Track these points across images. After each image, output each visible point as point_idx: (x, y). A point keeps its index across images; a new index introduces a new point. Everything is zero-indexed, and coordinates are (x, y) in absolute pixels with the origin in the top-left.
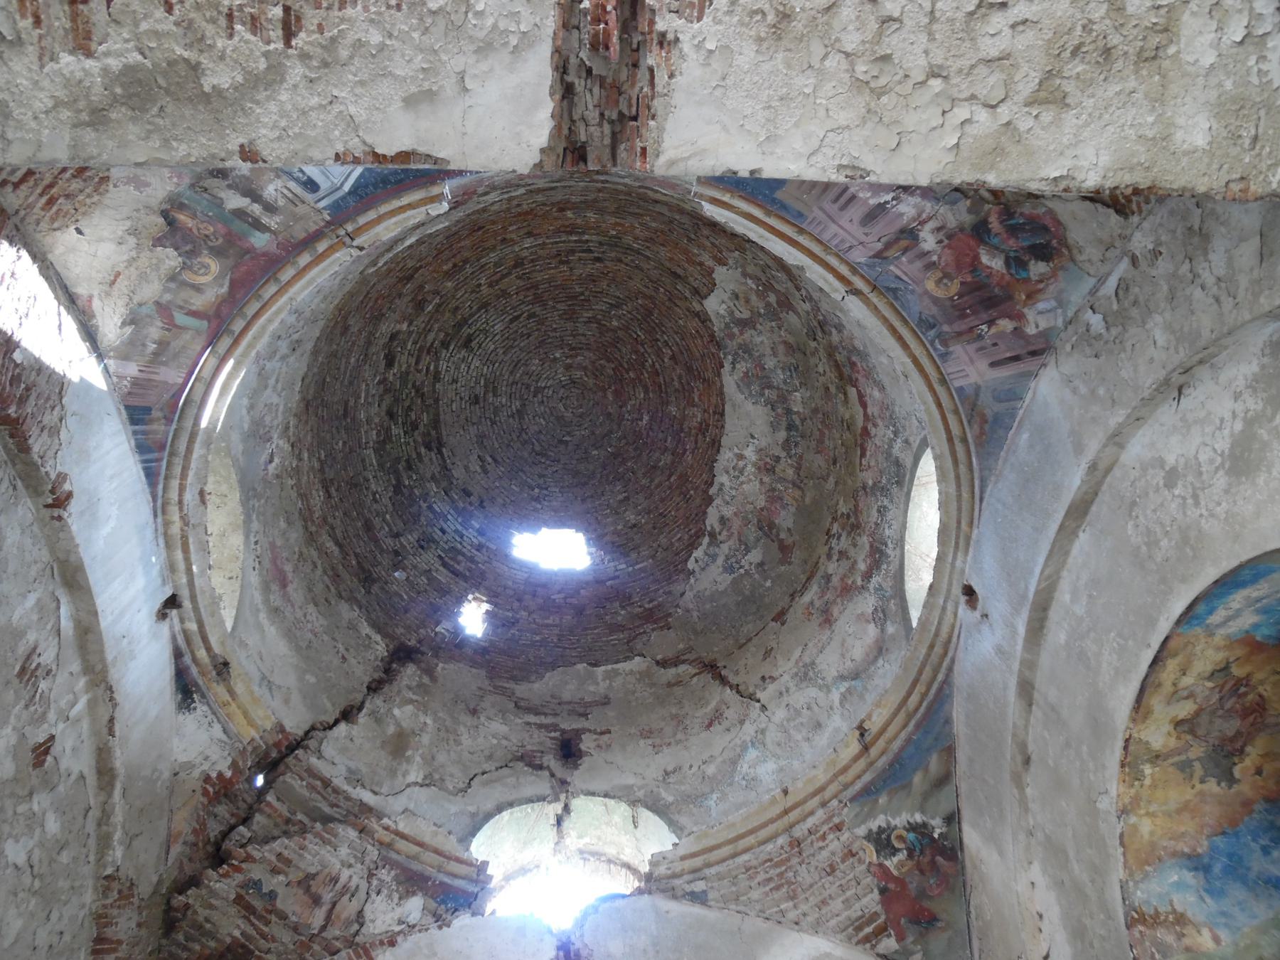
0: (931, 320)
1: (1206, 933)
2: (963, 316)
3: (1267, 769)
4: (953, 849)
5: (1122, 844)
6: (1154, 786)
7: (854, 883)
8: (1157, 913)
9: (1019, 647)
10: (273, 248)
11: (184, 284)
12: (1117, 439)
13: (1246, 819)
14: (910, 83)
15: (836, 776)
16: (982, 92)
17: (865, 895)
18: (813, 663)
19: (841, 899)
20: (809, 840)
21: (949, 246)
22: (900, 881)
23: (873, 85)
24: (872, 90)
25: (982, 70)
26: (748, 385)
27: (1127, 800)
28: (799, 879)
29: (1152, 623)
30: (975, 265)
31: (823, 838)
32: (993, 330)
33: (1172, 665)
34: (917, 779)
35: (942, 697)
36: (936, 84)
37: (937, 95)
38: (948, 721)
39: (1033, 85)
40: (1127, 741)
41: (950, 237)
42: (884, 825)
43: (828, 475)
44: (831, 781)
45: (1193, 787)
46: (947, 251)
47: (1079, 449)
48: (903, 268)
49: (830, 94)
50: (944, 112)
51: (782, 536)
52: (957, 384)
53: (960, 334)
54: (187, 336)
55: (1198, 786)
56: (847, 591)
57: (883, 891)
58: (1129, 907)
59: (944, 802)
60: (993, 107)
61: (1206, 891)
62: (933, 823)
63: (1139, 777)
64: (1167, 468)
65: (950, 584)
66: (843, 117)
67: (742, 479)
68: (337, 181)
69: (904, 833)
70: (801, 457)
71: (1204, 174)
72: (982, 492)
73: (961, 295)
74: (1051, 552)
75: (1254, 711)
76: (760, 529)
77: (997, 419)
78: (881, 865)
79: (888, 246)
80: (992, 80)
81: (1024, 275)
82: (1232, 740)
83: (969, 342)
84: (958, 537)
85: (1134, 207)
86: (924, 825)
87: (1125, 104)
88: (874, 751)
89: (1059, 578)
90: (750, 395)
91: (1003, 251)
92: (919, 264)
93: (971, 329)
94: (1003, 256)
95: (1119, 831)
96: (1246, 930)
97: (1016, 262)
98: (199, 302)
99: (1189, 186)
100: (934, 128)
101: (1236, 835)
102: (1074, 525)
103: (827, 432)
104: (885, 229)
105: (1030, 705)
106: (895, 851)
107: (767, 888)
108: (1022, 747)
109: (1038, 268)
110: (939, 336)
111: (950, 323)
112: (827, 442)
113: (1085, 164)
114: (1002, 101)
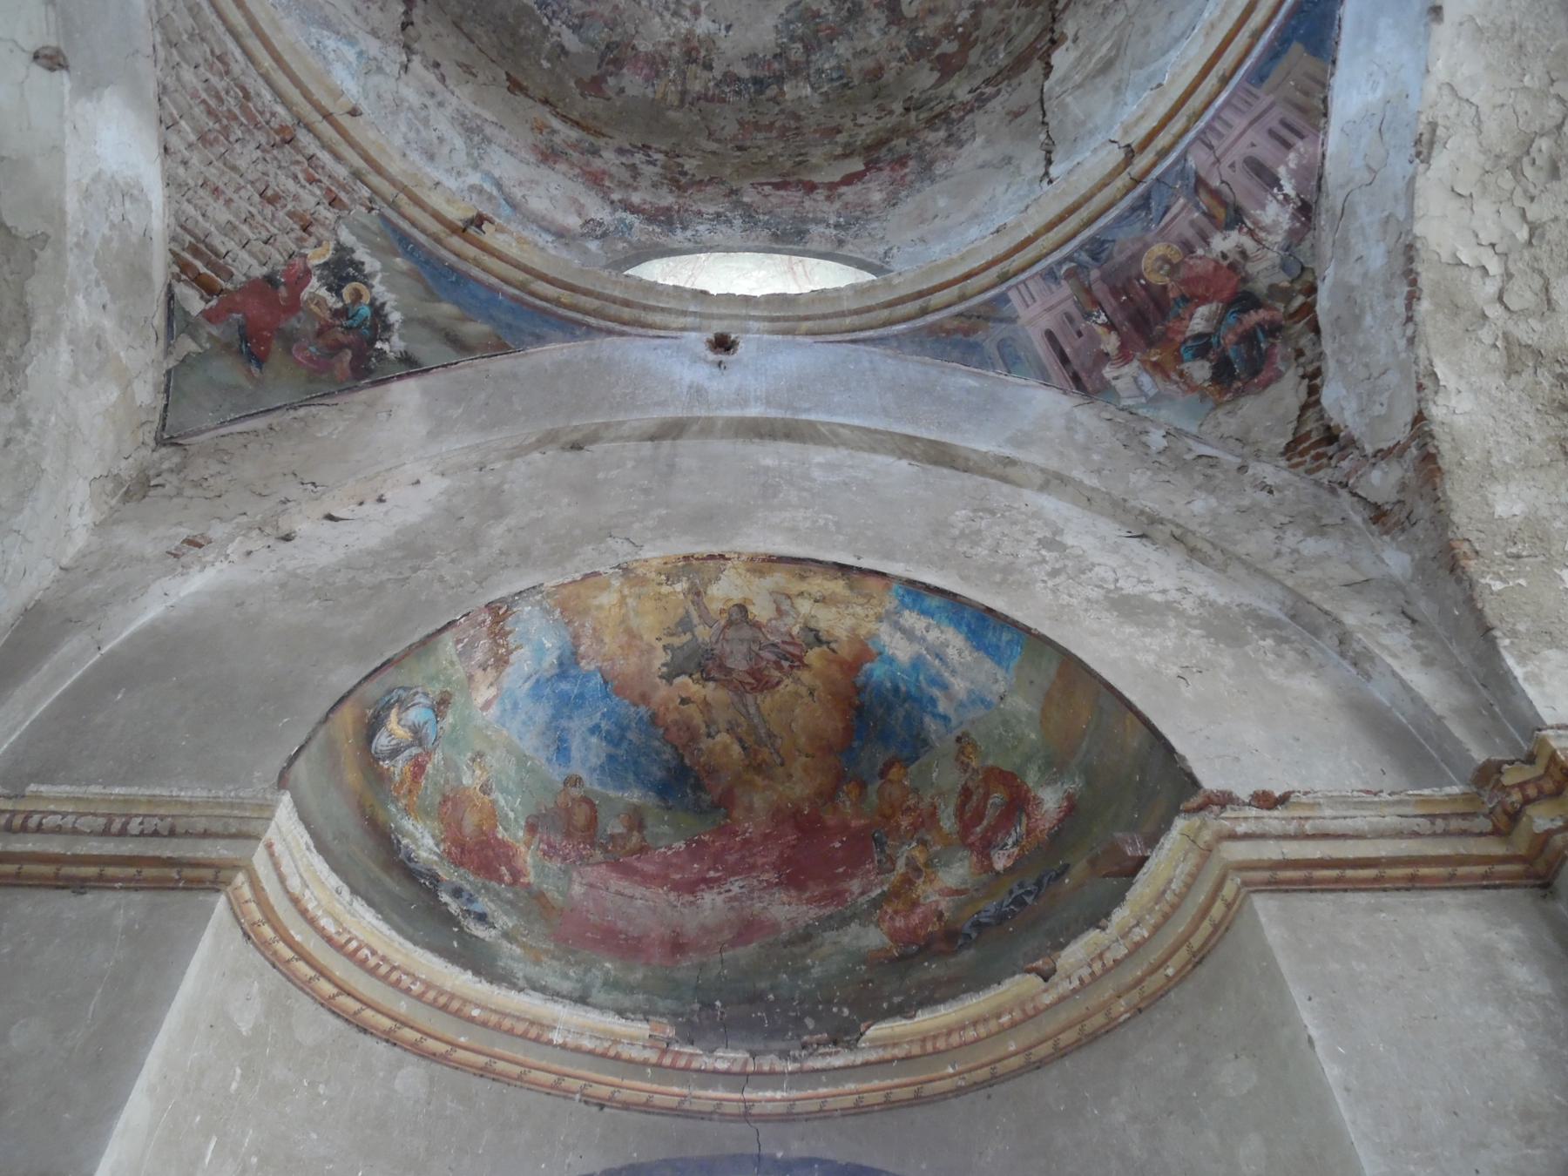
0: (1104, 256)
1: (492, 692)
2: (1115, 292)
3: (691, 710)
4: (369, 372)
5: (586, 577)
6: (659, 597)
7: (265, 235)
8: (506, 635)
9: (727, 413)
12: (1054, 482)
13: (627, 702)
14: (1525, 204)
15: (404, 189)
16: (1516, 285)
17: (252, 254)
18: (490, 141)
19: (232, 219)
20: (299, 158)
21: (1218, 267)
22: (294, 305)
23: (1526, 160)
24: (1518, 159)
25: (1537, 283)
26: (800, 18)
27: (640, 571)
28: (237, 147)
29: (888, 556)
30: (1191, 300)
31: (312, 180)
32: (1100, 330)
33: (838, 586)
34: (446, 309)
35: (571, 328)
36: (1523, 234)
37: (1513, 235)
38: (540, 339)
39: (1525, 339)
40: (722, 556)
41: (1232, 267)
42: (367, 269)
43: (718, 141)
44: (393, 182)
45: (659, 639)
46: (1211, 267)
47: (1019, 441)
48: (1183, 215)
49: (1518, 108)
50: (1493, 245)
51: (611, 81)
52: (1013, 295)
53: (1088, 291)
55: (660, 645)
56: (595, 180)
57: (270, 280)
58: (509, 603)
59: (427, 351)
60: (1500, 299)
61: (538, 681)
62: (395, 338)
63: (671, 578)
64: (1057, 538)
65: (721, 317)
66: (1491, 126)
67: (667, 16)
69: (366, 300)
70: (723, 101)
71: (1470, 518)
72: (864, 341)
73: (1147, 287)
74: (876, 431)
75: (759, 681)
76: (608, 47)
77: (974, 347)
78: (308, 273)
79: (1215, 194)
80: (1528, 295)
81: (1186, 356)
82: (722, 667)
83: (1077, 303)
84: (786, 319)
85: (1296, 460)
86: (388, 327)
87: (1518, 433)
88: (455, 241)
89: (835, 446)
90: (788, 22)
91: (1217, 329)
93: (1097, 303)
94: (1209, 330)
95: (602, 570)
96: (505, 732)
97: (1203, 346)
99: (1454, 506)
100: (1477, 236)
101: (607, 696)
102: (916, 452)
103: (774, 134)
104: (1241, 186)
105: (652, 438)
106: (336, 290)
107: (204, 96)
108: (594, 437)
109: (1200, 371)
110: (1080, 265)
111: (1103, 279)
112: (760, 136)
113: (1453, 403)
114: (1507, 308)
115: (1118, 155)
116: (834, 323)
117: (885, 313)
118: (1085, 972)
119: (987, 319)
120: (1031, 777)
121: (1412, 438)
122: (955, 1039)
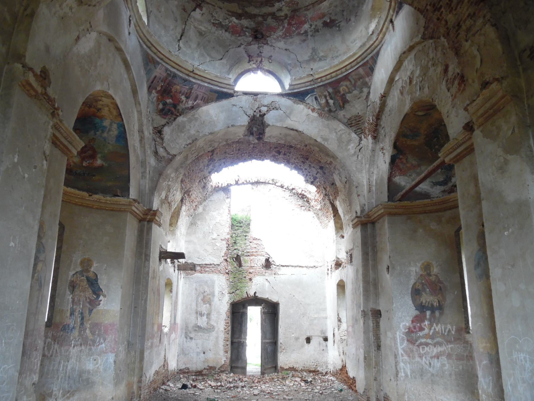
2: (168, 84)
10: (328, 87)
11: (348, 89)
30: (172, 98)
32: (160, 85)
46: (178, 98)
48: (185, 89)
52: (160, 65)
53: (166, 79)
54: (354, 77)
68: (311, 97)
74: (134, 79)
79: (191, 92)
81: (162, 102)
91: (169, 104)
92: (183, 92)
97: (165, 104)
98: (348, 83)
104: (193, 96)
109: (161, 106)
111: (170, 81)
115: (191, 69)
116: (140, 32)
117: (146, 40)
118: (96, 200)
119: (154, 63)
120: (99, 155)
121: (172, 155)
122: (70, 194)
